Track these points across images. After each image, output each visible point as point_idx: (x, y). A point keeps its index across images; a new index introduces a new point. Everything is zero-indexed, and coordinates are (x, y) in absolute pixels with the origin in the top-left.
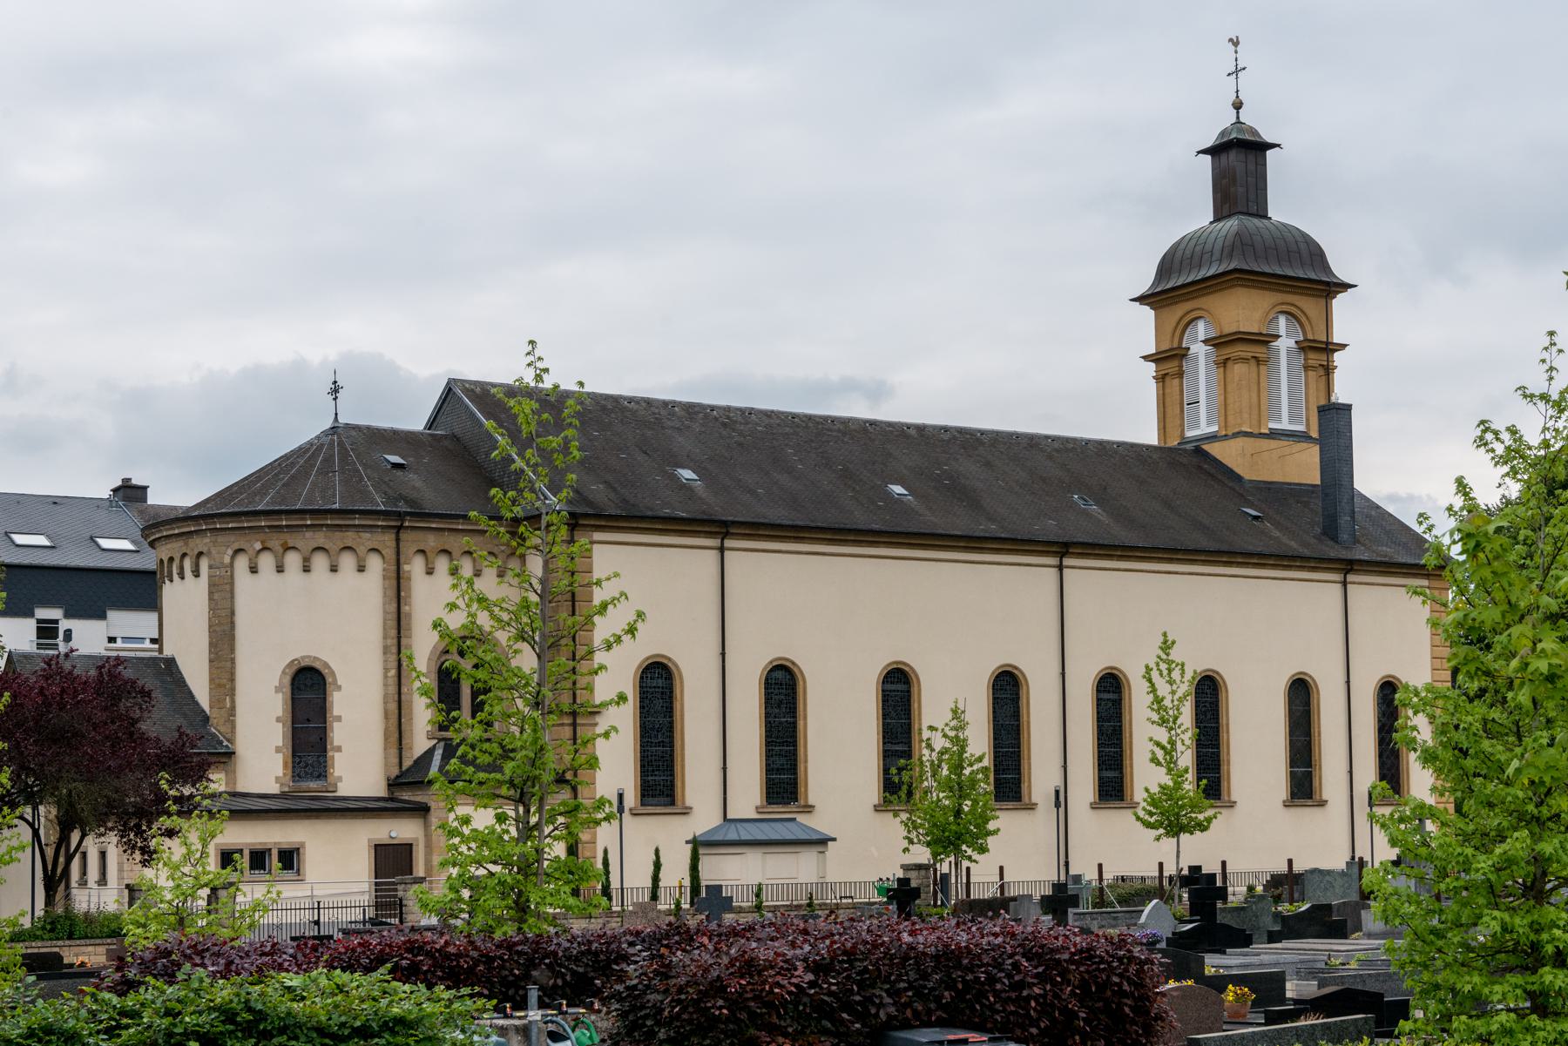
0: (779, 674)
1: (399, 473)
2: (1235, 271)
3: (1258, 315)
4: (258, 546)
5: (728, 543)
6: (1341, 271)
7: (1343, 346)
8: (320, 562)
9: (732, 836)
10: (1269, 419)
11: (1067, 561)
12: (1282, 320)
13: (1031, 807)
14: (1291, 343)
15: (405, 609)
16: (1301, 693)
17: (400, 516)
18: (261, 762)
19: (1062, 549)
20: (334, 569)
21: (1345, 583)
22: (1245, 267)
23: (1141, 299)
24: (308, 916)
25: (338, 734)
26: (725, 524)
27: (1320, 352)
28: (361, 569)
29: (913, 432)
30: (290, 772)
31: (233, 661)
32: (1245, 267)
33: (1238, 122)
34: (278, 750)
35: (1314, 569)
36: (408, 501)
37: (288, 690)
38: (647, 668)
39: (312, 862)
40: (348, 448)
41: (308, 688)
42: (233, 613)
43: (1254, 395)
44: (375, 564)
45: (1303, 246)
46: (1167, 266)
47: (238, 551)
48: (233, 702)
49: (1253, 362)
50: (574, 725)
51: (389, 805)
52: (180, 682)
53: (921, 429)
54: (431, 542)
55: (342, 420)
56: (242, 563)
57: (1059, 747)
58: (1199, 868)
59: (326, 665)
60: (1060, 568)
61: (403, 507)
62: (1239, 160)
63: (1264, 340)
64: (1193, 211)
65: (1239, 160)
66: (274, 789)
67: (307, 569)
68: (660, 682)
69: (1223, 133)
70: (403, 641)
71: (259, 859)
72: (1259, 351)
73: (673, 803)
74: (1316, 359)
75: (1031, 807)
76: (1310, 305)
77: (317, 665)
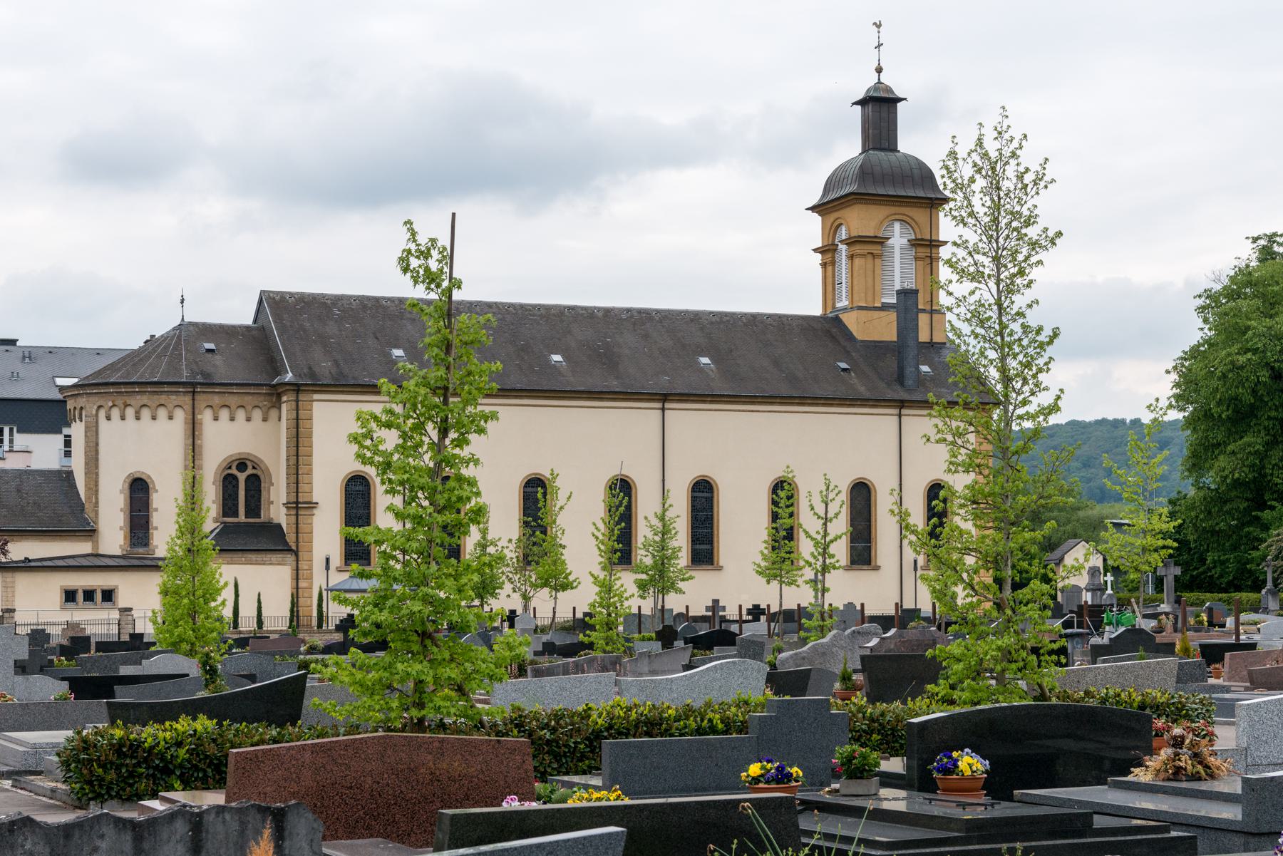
1: (210, 355)
4: (110, 404)
8: (146, 413)
10: (882, 296)
11: (667, 405)
12: (897, 226)
14: (905, 241)
15: (198, 442)
17: (193, 385)
18: (113, 538)
19: (664, 398)
21: (900, 416)
22: (882, 187)
23: (813, 209)
25: (156, 519)
29: (600, 314)
30: (128, 542)
31: (97, 474)
33: (879, 82)
36: (202, 373)
37: (127, 492)
38: (364, 478)
39: (57, 597)
40: (189, 336)
41: (139, 489)
42: (97, 444)
44: (180, 415)
45: (916, 172)
46: (830, 185)
47: (100, 407)
48: (97, 498)
49: (870, 257)
50: (297, 515)
52: (73, 485)
53: (608, 311)
54: (216, 400)
56: (102, 414)
57: (743, 527)
59: (149, 477)
60: (663, 409)
61: (199, 379)
62: (880, 108)
63: (880, 241)
64: (849, 148)
65: (880, 108)
66: (118, 552)
67: (138, 418)
68: (361, 488)
69: (868, 90)
71: (89, 595)
74: (923, 252)
76: (920, 215)
77: (143, 477)
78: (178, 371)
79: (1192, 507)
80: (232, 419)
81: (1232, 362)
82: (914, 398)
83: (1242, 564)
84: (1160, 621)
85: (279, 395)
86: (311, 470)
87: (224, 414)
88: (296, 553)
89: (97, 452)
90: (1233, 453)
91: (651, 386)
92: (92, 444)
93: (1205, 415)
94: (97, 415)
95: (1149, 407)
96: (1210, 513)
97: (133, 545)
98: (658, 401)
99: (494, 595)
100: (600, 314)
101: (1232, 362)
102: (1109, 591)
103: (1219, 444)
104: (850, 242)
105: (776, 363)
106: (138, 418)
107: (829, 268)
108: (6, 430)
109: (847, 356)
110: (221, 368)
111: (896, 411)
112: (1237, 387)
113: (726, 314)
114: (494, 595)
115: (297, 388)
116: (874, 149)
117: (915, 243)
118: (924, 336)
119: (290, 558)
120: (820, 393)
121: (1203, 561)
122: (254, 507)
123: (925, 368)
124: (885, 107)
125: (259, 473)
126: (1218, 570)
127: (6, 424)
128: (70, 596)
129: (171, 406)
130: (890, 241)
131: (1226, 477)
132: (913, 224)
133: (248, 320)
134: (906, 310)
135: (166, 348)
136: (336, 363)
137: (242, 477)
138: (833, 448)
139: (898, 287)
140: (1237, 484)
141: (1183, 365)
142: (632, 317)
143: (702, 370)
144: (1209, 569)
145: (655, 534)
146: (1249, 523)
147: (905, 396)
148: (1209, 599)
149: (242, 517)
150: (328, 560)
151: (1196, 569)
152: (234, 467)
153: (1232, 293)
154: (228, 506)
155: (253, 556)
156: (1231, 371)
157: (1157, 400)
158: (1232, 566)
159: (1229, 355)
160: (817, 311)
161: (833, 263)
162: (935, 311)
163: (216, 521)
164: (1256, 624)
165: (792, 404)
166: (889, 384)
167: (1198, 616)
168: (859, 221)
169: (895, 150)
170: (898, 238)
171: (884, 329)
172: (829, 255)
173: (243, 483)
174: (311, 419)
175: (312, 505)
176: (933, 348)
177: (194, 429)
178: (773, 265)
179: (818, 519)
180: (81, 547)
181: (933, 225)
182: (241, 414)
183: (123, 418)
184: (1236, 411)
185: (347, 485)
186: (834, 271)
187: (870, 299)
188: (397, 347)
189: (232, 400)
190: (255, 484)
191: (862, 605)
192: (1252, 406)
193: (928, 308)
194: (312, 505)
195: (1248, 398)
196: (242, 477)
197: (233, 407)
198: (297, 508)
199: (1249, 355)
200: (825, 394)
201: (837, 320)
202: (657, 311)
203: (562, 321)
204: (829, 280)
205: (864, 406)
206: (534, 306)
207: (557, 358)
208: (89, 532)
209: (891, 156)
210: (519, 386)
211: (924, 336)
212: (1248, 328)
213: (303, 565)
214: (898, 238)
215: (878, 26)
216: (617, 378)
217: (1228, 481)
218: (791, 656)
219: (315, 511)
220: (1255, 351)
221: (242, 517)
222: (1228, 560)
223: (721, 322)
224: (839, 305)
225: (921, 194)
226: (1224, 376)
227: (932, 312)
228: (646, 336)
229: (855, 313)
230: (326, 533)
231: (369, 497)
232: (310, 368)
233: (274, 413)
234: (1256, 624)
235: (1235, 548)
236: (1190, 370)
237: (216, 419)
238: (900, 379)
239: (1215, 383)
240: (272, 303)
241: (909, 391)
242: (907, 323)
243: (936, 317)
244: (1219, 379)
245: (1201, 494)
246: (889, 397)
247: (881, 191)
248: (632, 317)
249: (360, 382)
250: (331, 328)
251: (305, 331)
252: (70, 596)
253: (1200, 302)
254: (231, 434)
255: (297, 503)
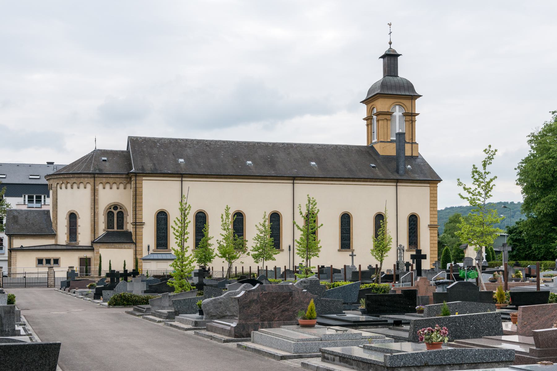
0: (201, 214)
1: (104, 162)
2: (377, 94)
3: (387, 106)
5: (184, 179)
6: (418, 91)
7: (418, 114)
8: (75, 186)
9: (152, 257)
11: (295, 182)
12: (397, 107)
13: (282, 250)
14: (401, 114)
15: (96, 198)
16: (380, 218)
17: (94, 174)
18: (63, 238)
19: (294, 178)
20: (111, 188)
21: (397, 186)
22: (393, 92)
24: (22, 276)
25: (79, 230)
26: (181, 174)
27: (410, 117)
28: (85, 188)
29: (271, 145)
30: (69, 239)
31: (57, 211)
32: (393, 92)
34: (79, 234)
35: (374, 182)
36: (99, 170)
37: (68, 218)
38: (165, 212)
39: (34, 262)
41: (73, 217)
42: (57, 199)
43: (386, 130)
44: (89, 187)
45: (405, 85)
47: (58, 184)
49: (385, 120)
50: (136, 228)
51: (68, 248)
53: (274, 144)
54: (104, 180)
55: (97, 148)
58: (323, 267)
60: (293, 183)
61: (97, 172)
62: (391, 59)
63: (390, 114)
65: (391, 59)
66: (65, 244)
67: (72, 188)
70: (96, 206)
71: (48, 261)
72: (388, 117)
73: (167, 248)
74: (409, 118)
75: (282, 250)
76: (407, 103)
77: (72, 212)
78: (89, 168)
79: (526, 225)
80: (111, 188)
81: (543, 163)
82: (403, 178)
83: (548, 249)
84: (494, 275)
85: (131, 178)
86: (142, 209)
87: (108, 186)
88: (135, 244)
89: (57, 202)
90: (544, 202)
91: (288, 173)
92: (55, 199)
93: (532, 186)
94: (57, 187)
95: (485, 151)
96: (533, 227)
97: (70, 240)
98: (291, 180)
99: (210, 261)
100: (271, 145)
101: (543, 163)
102: (485, 260)
103: (537, 198)
104: (378, 114)
105: (344, 164)
106: (72, 188)
107: (370, 126)
108: (43, 197)
109: (375, 161)
110: (107, 168)
111: (395, 184)
112: (545, 174)
113: (325, 145)
114: (210, 261)
115: (136, 175)
116: (388, 76)
117: (405, 115)
118: (408, 153)
119: (133, 246)
120: (362, 176)
121: (530, 247)
122: (121, 225)
123: (409, 166)
124: (392, 59)
125: (123, 211)
126: (537, 251)
127: (43, 194)
128: (40, 261)
129: (85, 183)
130: (394, 114)
131: (541, 212)
132: (404, 106)
133: (125, 149)
134: (400, 141)
135: (86, 160)
136: (154, 164)
137: (115, 212)
138: (365, 200)
139: (397, 132)
140: (545, 215)
141: (522, 166)
142: (284, 146)
143: (311, 167)
144: (533, 251)
145: (261, 233)
146: (551, 232)
147: (399, 177)
148: (531, 264)
149: (115, 229)
150: (149, 247)
151: (527, 251)
152: (112, 208)
153: (543, 135)
154: (110, 224)
155: (117, 245)
156: (542, 166)
157: (490, 146)
158: (543, 250)
159: (542, 160)
160: (365, 144)
161: (371, 124)
162: (413, 143)
163: (104, 230)
164: (552, 276)
165: (350, 181)
166: (392, 173)
167: (517, 272)
168: (381, 105)
169: (397, 76)
170: (398, 113)
171: (390, 150)
172: (370, 121)
173: (115, 214)
174: (142, 187)
175: (142, 224)
176: (413, 158)
177: (94, 192)
178: (349, 129)
179: (355, 228)
180: (51, 242)
181: (413, 106)
182: (115, 186)
183: (66, 188)
184: (545, 184)
185: (157, 215)
186: (371, 127)
187: (386, 138)
188: (181, 158)
189: (111, 181)
190: (121, 215)
191: (360, 266)
192: (552, 182)
193: (411, 142)
194: (142, 224)
195: (550, 179)
196: (115, 212)
197: (111, 183)
198: (136, 225)
199: (551, 160)
200: (364, 177)
201: (372, 147)
202: (295, 144)
203: (254, 148)
204: (370, 131)
205: (381, 182)
206: (243, 142)
207: (249, 162)
208: (54, 235)
209: (395, 79)
210: (231, 174)
211: (408, 153)
212: (550, 148)
213: (138, 249)
214: (398, 113)
215: (390, 25)
216: (274, 170)
217: (542, 214)
218: (211, 301)
219: (144, 226)
220: (553, 158)
221: (115, 229)
222: (541, 247)
223: (322, 148)
224: (373, 141)
225: (407, 93)
226: (540, 169)
227: (412, 143)
228: (289, 154)
229: (379, 144)
230: (148, 236)
231: (167, 220)
232: (143, 167)
233: (128, 186)
234: (552, 276)
235: (544, 242)
236: (525, 168)
237: (104, 188)
238: (397, 171)
239: (535, 172)
240: (133, 141)
241: (401, 175)
242: (400, 148)
243: (414, 145)
244: (537, 170)
245: (530, 219)
246: (392, 178)
247: (390, 92)
248: (284, 146)
249: (163, 172)
250: (155, 151)
251: (144, 152)
252: (40, 261)
253: (529, 138)
254: (111, 195)
255: (136, 223)
